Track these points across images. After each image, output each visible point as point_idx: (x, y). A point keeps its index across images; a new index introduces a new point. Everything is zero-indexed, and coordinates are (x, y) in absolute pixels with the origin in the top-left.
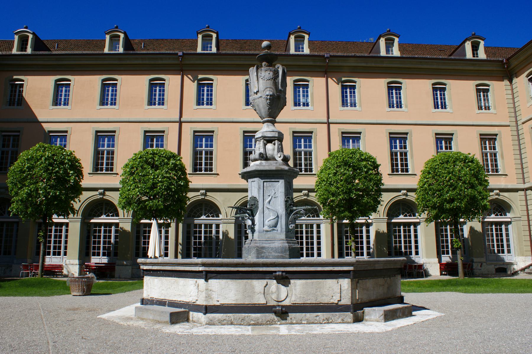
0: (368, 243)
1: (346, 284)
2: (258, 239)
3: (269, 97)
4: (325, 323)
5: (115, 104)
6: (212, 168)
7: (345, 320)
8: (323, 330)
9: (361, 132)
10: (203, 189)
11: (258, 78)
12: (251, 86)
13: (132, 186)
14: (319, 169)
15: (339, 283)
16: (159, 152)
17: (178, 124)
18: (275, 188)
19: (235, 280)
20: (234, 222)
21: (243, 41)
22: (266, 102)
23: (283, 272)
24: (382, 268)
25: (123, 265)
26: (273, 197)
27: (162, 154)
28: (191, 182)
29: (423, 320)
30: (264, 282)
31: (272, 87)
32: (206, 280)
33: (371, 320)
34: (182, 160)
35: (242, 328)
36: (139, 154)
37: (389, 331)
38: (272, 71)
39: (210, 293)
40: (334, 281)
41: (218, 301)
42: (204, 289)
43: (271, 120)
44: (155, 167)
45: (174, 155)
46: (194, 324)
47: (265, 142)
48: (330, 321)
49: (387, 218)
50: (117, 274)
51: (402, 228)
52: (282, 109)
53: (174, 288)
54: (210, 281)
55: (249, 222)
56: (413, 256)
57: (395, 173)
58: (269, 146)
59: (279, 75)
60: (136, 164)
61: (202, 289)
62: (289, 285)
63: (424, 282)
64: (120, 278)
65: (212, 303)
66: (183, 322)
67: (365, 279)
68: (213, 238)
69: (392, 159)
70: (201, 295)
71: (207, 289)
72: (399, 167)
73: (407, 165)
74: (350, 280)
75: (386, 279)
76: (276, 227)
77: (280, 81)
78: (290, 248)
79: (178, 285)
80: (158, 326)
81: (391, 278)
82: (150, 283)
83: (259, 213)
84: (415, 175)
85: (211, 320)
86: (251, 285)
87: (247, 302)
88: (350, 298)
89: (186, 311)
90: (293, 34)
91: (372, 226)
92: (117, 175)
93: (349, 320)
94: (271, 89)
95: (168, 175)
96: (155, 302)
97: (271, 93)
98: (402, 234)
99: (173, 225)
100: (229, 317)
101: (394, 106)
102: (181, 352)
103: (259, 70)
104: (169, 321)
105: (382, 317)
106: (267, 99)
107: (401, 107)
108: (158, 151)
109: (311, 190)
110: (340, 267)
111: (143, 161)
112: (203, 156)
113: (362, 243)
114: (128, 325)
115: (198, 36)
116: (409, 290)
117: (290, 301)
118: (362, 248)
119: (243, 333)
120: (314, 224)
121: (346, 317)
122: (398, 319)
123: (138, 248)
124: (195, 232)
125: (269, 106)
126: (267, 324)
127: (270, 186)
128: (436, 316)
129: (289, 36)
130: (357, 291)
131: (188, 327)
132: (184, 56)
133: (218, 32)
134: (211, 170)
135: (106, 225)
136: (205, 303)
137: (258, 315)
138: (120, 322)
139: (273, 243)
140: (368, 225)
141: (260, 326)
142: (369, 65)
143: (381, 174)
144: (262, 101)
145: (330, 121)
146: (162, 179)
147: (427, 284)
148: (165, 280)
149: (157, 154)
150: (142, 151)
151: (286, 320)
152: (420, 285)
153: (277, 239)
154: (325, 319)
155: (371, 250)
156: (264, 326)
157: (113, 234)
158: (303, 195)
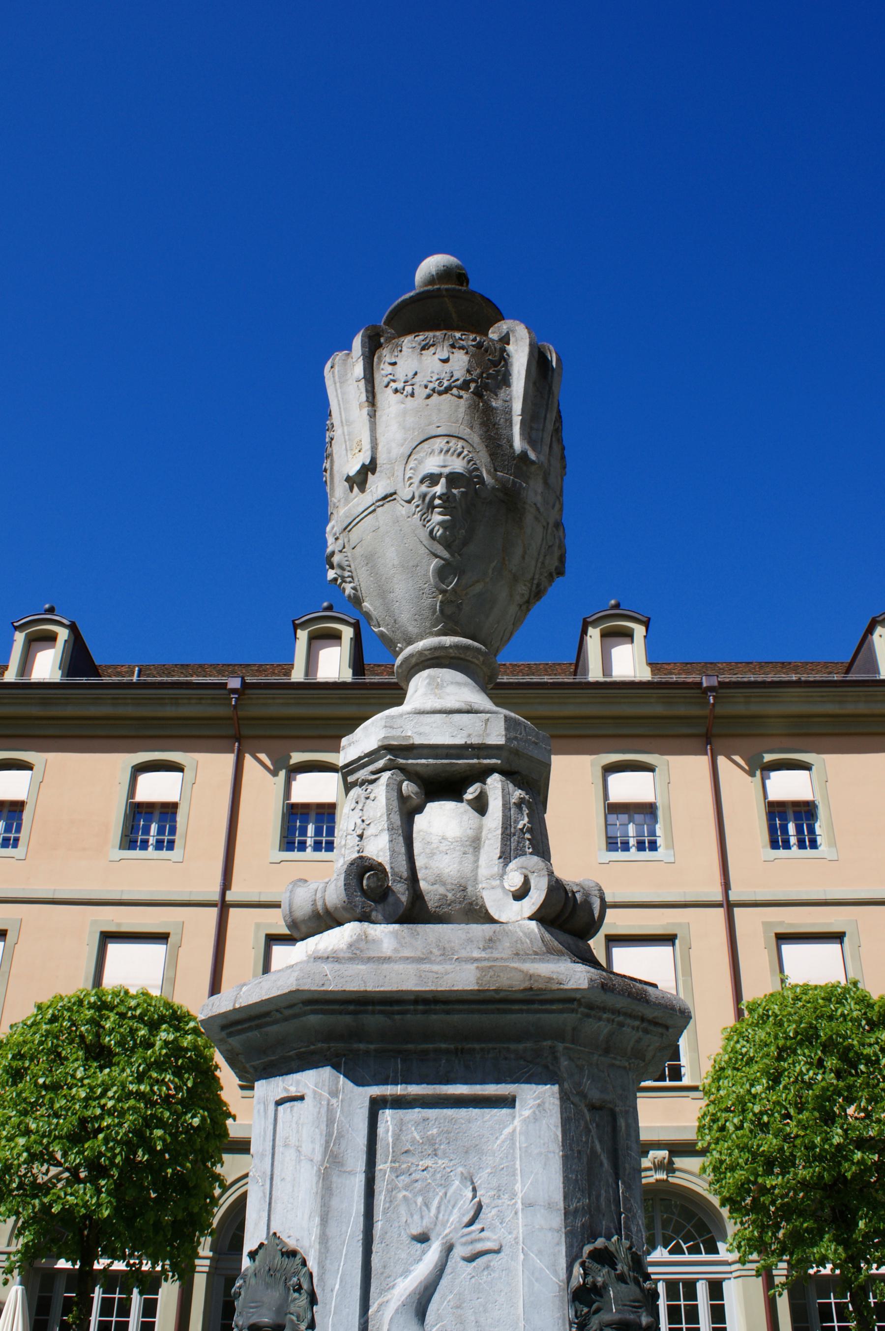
14: (707, 1067)
16: (122, 1001)
17: (214, 912)
18: (473, 1159)
22: (425, 521)
26: (460, 1251)
27: (130, 1008)
28: (234, 1119)
31: (465, 432)
36: (49, 1007)
38: (462, 348)
43: (456, 647)
45: (175, 1012)
47: (408, 787)
77: (517, 406)
90: (595, 623)
97: (458, 465)
106: (431, 507)
127: (430, 1141)
129: (584, 632)
132: (248, 691)
133: (358, 621)
142: (850, 709)
144: (396, 521)
145: (733, 897)
146: (119, 1100)
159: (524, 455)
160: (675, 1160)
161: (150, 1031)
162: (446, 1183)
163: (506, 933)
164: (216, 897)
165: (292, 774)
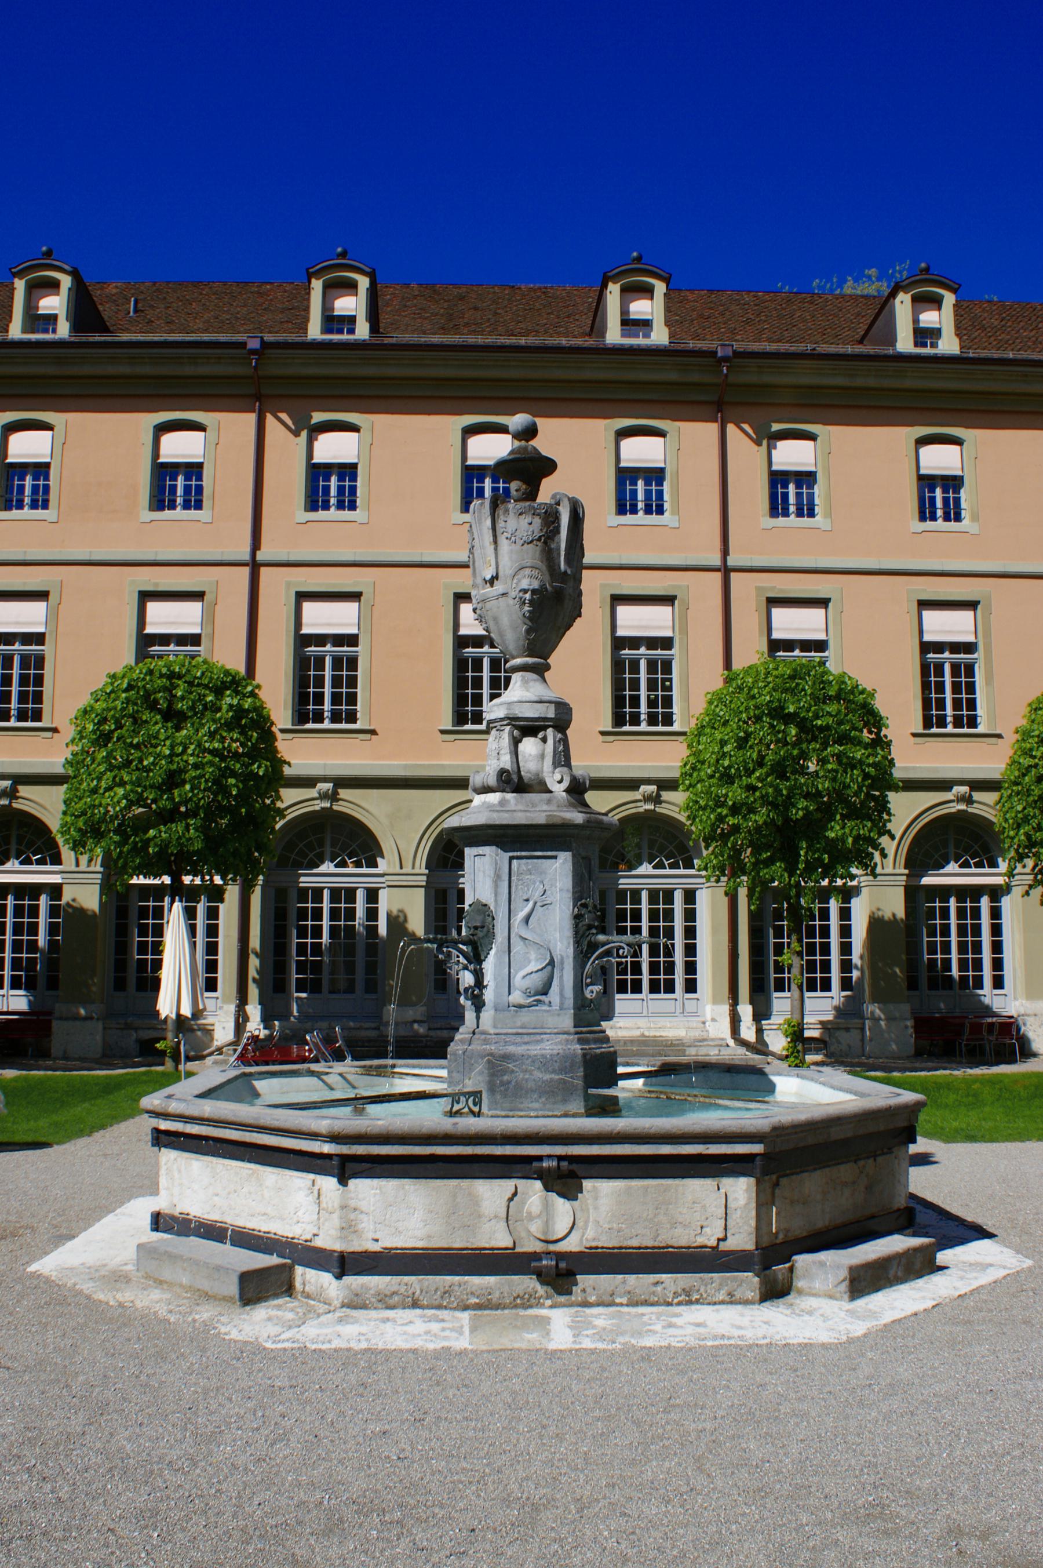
0: (846, 948)
1: (741, 1192)
2: (492, 1031)
3: (528, 596)
4: (679, 1304)
5: (45, 506)
6: (355, 712)
7: (738, 1295)
8: (671, 1331)
9: (829, 600)
10: (325, 779)
11: (495, 536)
12: (476, 559)
13: (105, 777)
14: (693, 723)
15: (722, 1191)
16: (188, 671)
19: (424, 1180)
20: (424, 884)
21: (456, 291)
22: (521, 609)
23: (560, 1158)
24: (849, 1134)
25: (77, 1018)
26: (539, 904)
27: (196, 678)
29: (962, 1292)
30: (504, 1187)
32: (343, 1181)
33: (814, 1292)
34: (262, 694)
35: (443, 1320)
36: (124, 676)
37: (858, 1338)
39: (352, 1216)
40: (709, 1183)
41: (377, 1240)
42: (336, 1205)
44: (173, 717)
45: (234, 677)
46: (307, 1303)
47: (516, 733)
48: (695, 1297)
49: (906, 871)
50: (56, 1046)
51: (953, 903)
52: (569, 626)
53: (250, 1193)
54: (353, 1183)
55: (467, 979)
56: (987, 993)
57: (934, 730)
58: (529, 746)
59: (559, 526)
60: (115, 708)
61: (330, 1205)
62: (580, 1195)
63: (1015, 1079)
64: (66, 1058)
65: (360, 1245)
66: (276, 1296)
67: (797, 1173)
68: (359, 932)
69: (925, 686)
70: (326, 1220)
71: (343, 1207)
72: (949, 711)
73: (972, 704)
74: (752, 1181)
75: (861, 1163)
76: (545, 994)
77: (563, 546)
78: (588, 1057)
79: (261, 1185)
80: (205, 1313)
81: (879, 1159)
82: (180, 1171)
83: (497, 951)
84: (999, 736)
85: (357, 1295)
86: (470, 1194)
87: (458, 1242)
88: (753, 1230)
89: (284, 1265)
90: (615, 279)
91: (858, 896)
92: (56, 735)
93: (750, 1295)
94: (535, 572)
95: (216, 745)
96: (193, 1225)
97: (536, 585)
98: (953, 921)
99: (232, 893)
100: (406, 1285)
101: (935, 513)
102: (276, 1424)
103: (500, 511)
104: (237, 1297)
105: (844, 1287)
106: (524, 603)
107: (958, 518)
108: (184, 666)
109: (667, 785)
110: (724, 1146)
111: (137, 699)
112: (328, 673)
113: (826, 949)
114: (121, 1305)
115: (310, 282)
116: (956, 1131)
117: (581, 1240)
118: (826, 966)
119: (446, 1344)
120: (676, 889)
121: (740, 1285)
122: (891, 1286)
123: (121, 965)
124: (302, 914)
125: (527, 621)
126: (516, 1307)
127: (529, 870)
128: (1007, 1272)
129: (604, 286)
130: (774, 1209)
131: (290, 1315)
132: (266, 351)
133: (374, 270)
134: (352, 717)
135: (22, 890)
136: (338, 1246)
137: (491, 1280)
138: (95, 1292)
139: (538, 1042)
140: (847, 894)
141: (494, 1312)
142: (859, 382)
143: (889, 744)
144: (508, 606)
145: (731, 562)
147: (1025, 1088)
148: (221, 1167)
149: (180, 677)
150: (133, 663)
151: (570, 1293)
152: (1001, 1089)
153: (548, 1031)
154: (680, 1291)
155: (855, 974)
156: (506, 1311)
157: (43, 920)
158: (640, 797)
159: (565, 572)
160: (663, 793)
161: (216, 696)
162: (534, 883)
163: (554, 797)
164: (246, 557)
165: (314, 434)
